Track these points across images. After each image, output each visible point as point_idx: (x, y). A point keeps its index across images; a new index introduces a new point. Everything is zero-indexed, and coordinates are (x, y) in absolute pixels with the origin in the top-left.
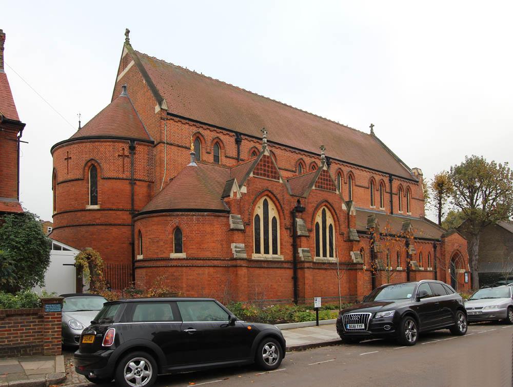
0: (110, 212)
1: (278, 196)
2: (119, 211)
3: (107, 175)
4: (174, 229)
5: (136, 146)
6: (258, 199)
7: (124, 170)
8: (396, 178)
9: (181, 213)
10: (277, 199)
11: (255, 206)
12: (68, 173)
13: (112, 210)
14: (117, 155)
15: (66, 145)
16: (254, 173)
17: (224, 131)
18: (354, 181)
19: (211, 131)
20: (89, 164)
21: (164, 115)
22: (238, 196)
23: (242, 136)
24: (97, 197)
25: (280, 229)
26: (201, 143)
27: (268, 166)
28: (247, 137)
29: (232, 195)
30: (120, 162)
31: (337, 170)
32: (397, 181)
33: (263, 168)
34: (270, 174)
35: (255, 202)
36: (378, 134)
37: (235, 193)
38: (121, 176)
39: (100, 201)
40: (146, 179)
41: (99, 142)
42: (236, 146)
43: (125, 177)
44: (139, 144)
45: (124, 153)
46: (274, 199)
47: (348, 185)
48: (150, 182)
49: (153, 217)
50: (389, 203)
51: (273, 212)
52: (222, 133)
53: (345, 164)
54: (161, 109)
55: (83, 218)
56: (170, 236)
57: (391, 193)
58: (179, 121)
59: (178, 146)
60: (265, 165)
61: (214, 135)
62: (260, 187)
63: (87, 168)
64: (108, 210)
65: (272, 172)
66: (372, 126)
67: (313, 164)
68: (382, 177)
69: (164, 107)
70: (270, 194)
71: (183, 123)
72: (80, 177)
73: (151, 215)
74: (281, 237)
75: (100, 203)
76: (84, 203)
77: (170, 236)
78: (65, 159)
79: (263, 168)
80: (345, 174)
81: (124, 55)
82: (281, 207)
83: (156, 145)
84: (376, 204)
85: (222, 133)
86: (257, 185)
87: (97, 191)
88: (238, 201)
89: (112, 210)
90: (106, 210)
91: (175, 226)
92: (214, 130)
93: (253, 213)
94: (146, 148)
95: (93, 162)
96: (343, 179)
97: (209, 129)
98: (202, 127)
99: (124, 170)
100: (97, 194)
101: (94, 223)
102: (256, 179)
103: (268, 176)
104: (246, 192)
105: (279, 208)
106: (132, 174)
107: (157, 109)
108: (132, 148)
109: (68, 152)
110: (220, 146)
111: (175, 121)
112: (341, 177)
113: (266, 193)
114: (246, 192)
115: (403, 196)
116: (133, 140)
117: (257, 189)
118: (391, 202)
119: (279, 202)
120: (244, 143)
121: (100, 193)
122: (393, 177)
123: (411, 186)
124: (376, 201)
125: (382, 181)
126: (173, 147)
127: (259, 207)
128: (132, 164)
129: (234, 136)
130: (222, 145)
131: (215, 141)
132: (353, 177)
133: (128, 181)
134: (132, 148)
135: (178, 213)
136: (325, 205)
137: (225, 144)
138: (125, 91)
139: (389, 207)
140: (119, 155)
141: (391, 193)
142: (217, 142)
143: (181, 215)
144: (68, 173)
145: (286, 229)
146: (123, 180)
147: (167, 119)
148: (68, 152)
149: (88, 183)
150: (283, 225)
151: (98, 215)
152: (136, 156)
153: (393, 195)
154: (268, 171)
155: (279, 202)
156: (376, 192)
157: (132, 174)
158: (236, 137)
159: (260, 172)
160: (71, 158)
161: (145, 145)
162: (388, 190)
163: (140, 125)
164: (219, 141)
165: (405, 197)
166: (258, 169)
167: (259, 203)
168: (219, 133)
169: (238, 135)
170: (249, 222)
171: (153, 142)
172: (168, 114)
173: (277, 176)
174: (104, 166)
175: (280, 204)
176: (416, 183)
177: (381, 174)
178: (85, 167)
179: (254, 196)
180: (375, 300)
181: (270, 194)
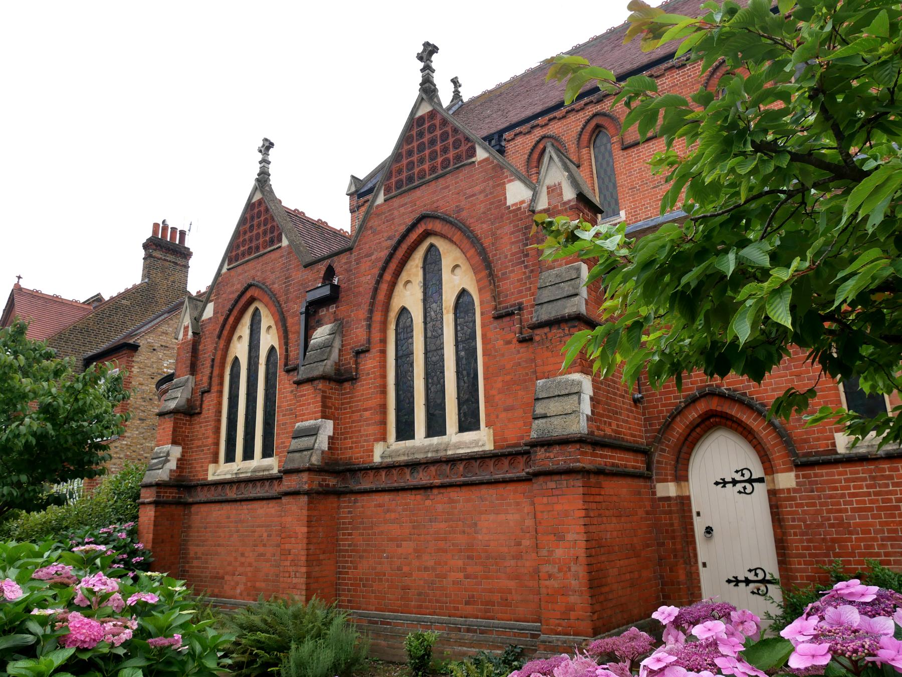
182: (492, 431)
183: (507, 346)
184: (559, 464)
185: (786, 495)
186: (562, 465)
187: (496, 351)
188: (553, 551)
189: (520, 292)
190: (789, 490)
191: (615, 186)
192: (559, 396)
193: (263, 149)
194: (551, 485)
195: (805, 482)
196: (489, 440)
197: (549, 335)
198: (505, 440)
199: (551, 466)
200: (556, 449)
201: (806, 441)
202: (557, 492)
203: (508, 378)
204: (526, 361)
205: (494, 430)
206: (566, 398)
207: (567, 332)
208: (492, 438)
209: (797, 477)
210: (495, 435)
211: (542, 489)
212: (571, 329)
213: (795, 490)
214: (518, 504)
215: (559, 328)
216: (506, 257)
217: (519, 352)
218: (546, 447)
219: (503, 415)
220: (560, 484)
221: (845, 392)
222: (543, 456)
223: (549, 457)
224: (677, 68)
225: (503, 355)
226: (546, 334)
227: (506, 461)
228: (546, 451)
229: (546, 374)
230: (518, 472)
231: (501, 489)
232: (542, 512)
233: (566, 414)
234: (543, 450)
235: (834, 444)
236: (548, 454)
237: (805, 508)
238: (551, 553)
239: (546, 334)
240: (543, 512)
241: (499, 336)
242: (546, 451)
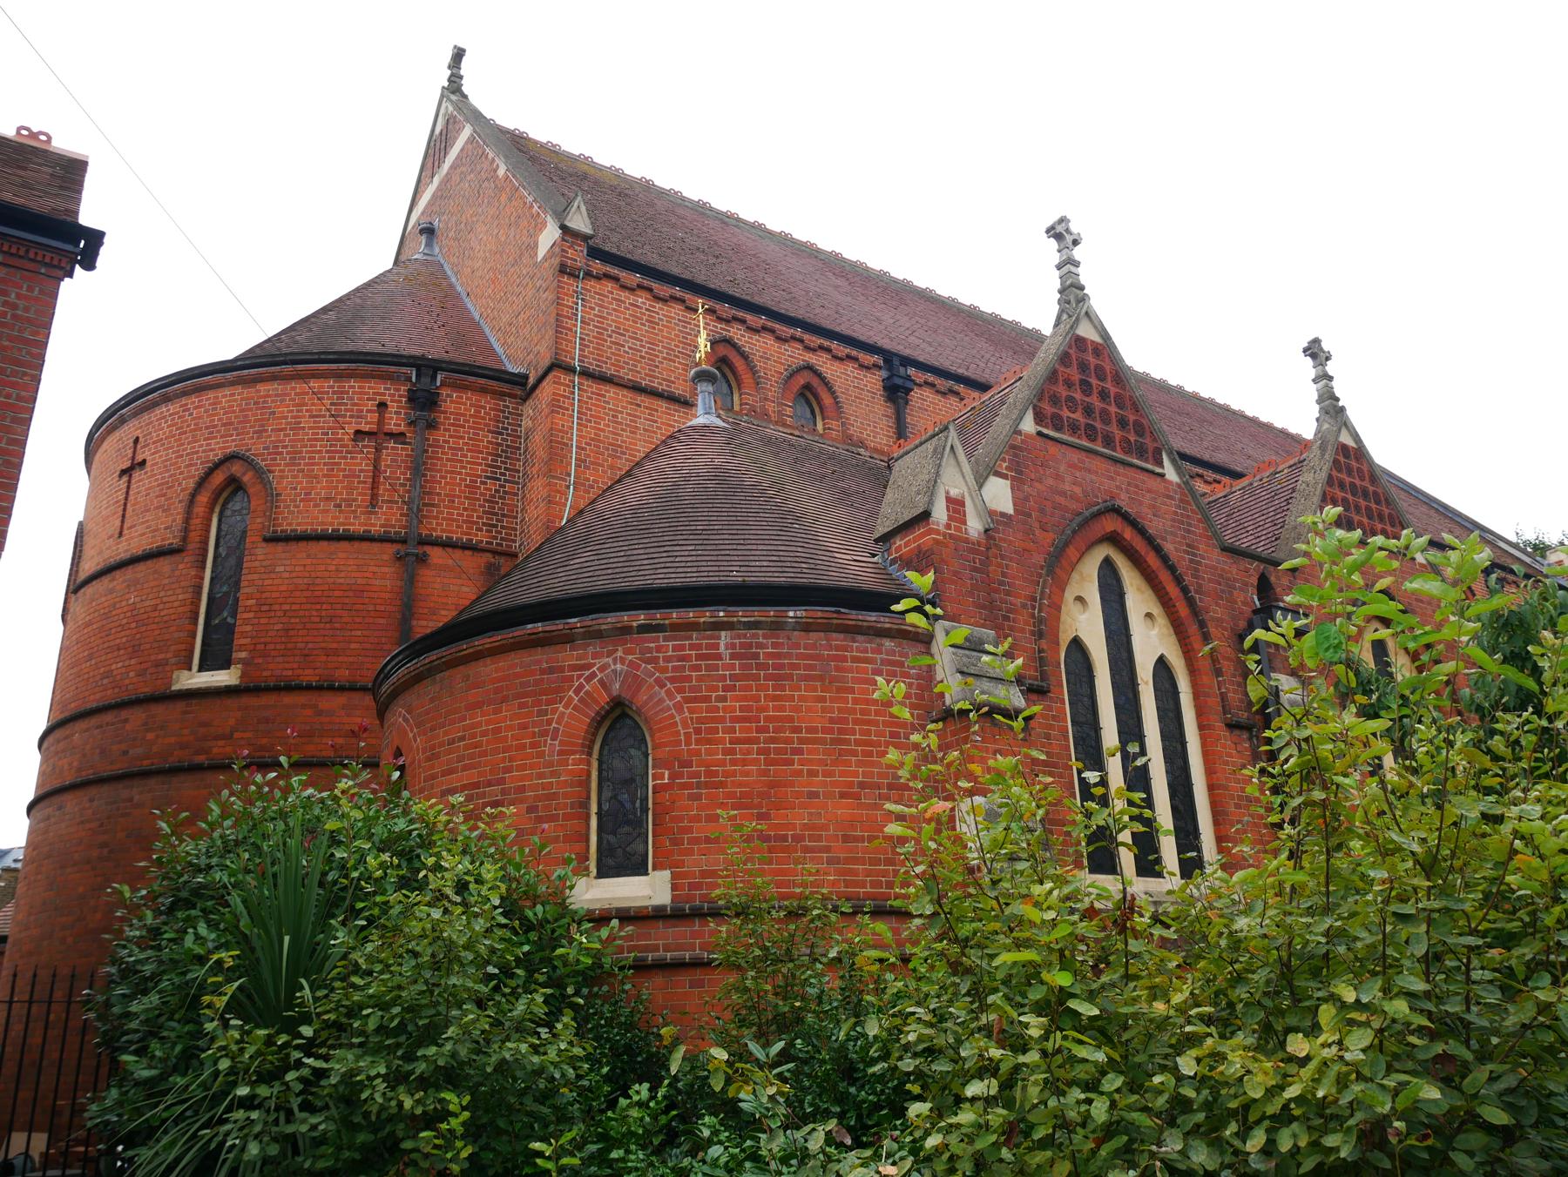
0: (288, 699)
1: (1169, 547)
2: (328, 695)
3: (294, 519)
4: (598, 721)
5: (444, 392)
6: (1072, 552)
7: (374, 496)
9: (641, 618)
10: (1164, 558)
11: (1061, 587)
12: (121, 534)
13: (299, 688)
14: (353, 428)
15: (136, 414)
16: (1039, 418)
17: (834, 345)
19: (779, 339)
20: (219, 478)
21: (578, 256)
22: (974, 526)
23: (911, 371)
24: (230, 630)
25: (1201, 727)
27: (1104, 395)
28: (931, 378)
29: (940, 514)
30: (362, 464)
33: (1078, 396)
34: (1117, 433)
35: (1058, 566)
37: (956, 505)
38: (357, 527)
39: (241, 648)
40: (480, 537)
41: (273, 378)
42: (890, 411)
43: (376, 525)
44: (463, 388)
45: (381, 422)
46: (1152, 560)
48: (495, 553)
49: (478, 656)
51: (1155, 632)
54: (564, 228)
55: (150, 736)
56: (574, 763)
58: (640, 286)
59: (637, 388)
60: (1086, 387)
61: (794, 355)
62: (1078, 490)
63: (203, 498)
64: (277, 689)
65: (1122, 423)
69: (580, 222)
70: (1128, 534)
71: (657, 298)
72: (172, 540)
73: (467, 647)
74: (1210, 771)
75: (243, 655)
76: (165, 663)
77: (574, 763)
78: (123, 472)
79: (1078, 396)
81: (437, 131)
82: (1191, 602)
83: (535, 387)
85: (828, 350)
86: (1058, 477)
87: (237, 600)
88: (972, 547)
89: (299, 688)
90: (268, 689)
91: (604, 698)
92: (793, 338)
93: (1057, 636)
94: (487, 402)
95: (236, 468)
97: (772, 331)
98: (743, 321)
99: (374, 496)
100: (234, 614)
101: (200, 759)
102: (1053, 449)
103: (1108, 441)
104: (1011, 511)
105: (1183, 610)
106: (417, 509)
107: (549, 235)
108: (424, 403)
109: (137, 441)
111: (624, 287)
113: (1111, 524)
114: (1011, 511)
116: (426, 366)
117: (1062, 500)
119: (1178, 580)
120: (922, 398)
121: (248, 609)
126: (611, 392)
127: (1080, 599)
128: (419, 468)
129: (876, 366)
130: (827, 400)
131: (801, 380)
133: (391, 549)
134: (424, 403)
135: (625, 617)
136: (1114, 539)
138: (429, 244)
140: (358, 432)
142: (807, 387)
143: (644, 629)
144: (121, 534)
145: (1232, 726)
146: (365, 545)
147: (588, 274)
148: (137, 441)
149: (203, 568)
150: (1214, 702)
151: (227, 715)
152: (440, 436)
154: (1105, 417)
155: (1178, 580)
157: (417, 509)
158: (884, 374)
159: (1066, 413)
160: (144, 462)
161: (484, 390)
163: (468, 330)
164: (815, 382)
166: (1055, 400)
167: (1075, 575)
168: (814, 350)
169: (896, 362)
170: (1044, 676)
171: (519, 380)
172: (595, 253)
173: (1150, 445)
174: (286, 480)
175: (1185, 590)
178: (193, 496)
179: (1047, 539)
181: (1128, 534)
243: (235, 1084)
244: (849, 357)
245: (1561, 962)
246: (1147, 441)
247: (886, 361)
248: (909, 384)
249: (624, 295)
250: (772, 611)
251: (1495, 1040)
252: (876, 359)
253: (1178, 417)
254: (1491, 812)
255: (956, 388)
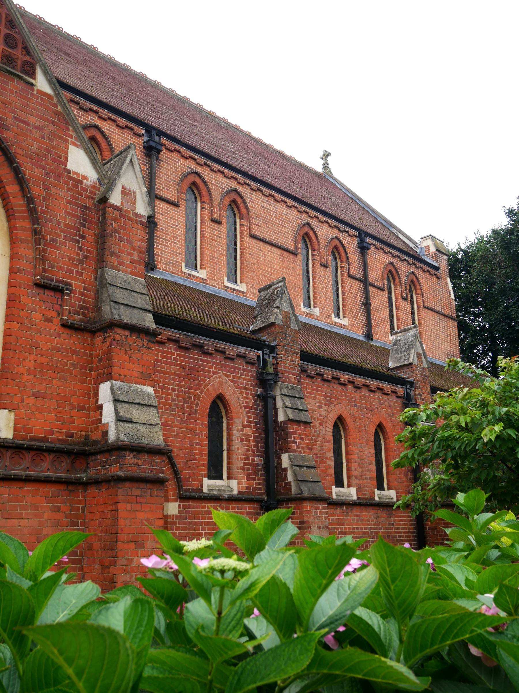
8: (379, 245)
18: (245, 222)
23: (163, 140)
26: (416, 290)
31: (387, 266)
32: (381, 253)
36: (336, 174)
47: (331, 269)
50: (361, 309)
52: (285, 202)
53: (216, 166)
57: (365, 281)
66: (326, 155)
67: (306, 229)
68: (335, 233)
80: (216, 194)
84: (348, 312)
96: (207, 206)
110: (200, 194)
112: (202, 202)
115: (399, 297)
118: (367, 304)
122: (368, 239)
123: (419, 274)
124: (321, 296)
125: (337, 242)
132: (244, 211)
137: (252, 211)
139: (361, 319)
141: (365, 281)
142: (194, 183)
153: (372, 290)
156: (320, 270)
158: (145, 139)
162: (356, 271)
165: (405, 299)
169: (363, 235)
176: (433, 271)
177: (333, 222)
180: (122, 632)
182: (13, 416)
183: (46, 323)
184: (145, 472)
185: (171, 520)
186: (148, 474)
187: (31, 322)
188: (132, 559)
189: (70, 271)
190: (173, 516)
191: (186, 240)
192: (139, 404)
193: (324, 157)
194: (137, 492)
195: (183, 511)
196: (8, 425)
197: (129, 338)
198: (31, 431)
199: (138, 473)
200: (145, 457)
201: (188, 480)
202: (142, 500)
203: (42, 360)
204: (67, 350)
205: (16, 415)
206: (145, 409)
207: (146, 344)
208: (12, 424)
209: (179, 506)
210: (16, 422)
211: (127, 495)
212: (150, 343)
213: (177, 517)
214: (36, 508)
215: (139, 337)
216: (59, 223)
217: (59, 336)
218: (135, 453)
219: (31, 401)
220: (145, 492)
221: (342, 463)
222: (131, 462)
223: (137, 464)
224: (134, 133)
225: (39, 331)
226: (126, 337)
227: (29, 456)
228: (135, 457)
229: (122, 377)
230: (42, 471)
231: (16, 488)
232: (125, 519)
233: (150, 425)
234: (132, 455)
235: (202, 486)
236: (136, 461)
237: (181, 531)
238: (130, 561)
239: (126, 337)
240: (127, 519)
241: (37, 307)
242: (135, 457)
243: (478, 296)
244: (127, 127)
245: (296, 633)
246: (18, 53)
247: (147, 131)
248: (159, 147)
249: (225, 179)
250: (334, 330)
251: (472, 318)
252: (352, 232)
253: (187, 119)
254: (21, 576)
255: (209, 163)
